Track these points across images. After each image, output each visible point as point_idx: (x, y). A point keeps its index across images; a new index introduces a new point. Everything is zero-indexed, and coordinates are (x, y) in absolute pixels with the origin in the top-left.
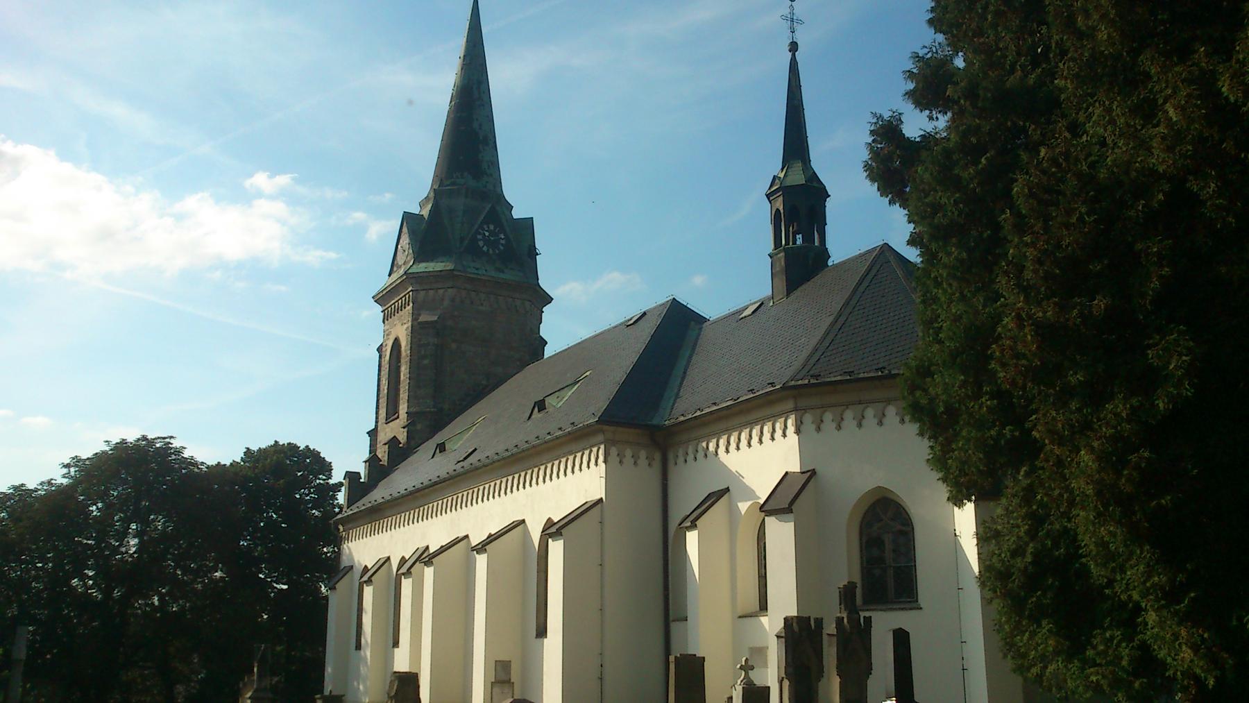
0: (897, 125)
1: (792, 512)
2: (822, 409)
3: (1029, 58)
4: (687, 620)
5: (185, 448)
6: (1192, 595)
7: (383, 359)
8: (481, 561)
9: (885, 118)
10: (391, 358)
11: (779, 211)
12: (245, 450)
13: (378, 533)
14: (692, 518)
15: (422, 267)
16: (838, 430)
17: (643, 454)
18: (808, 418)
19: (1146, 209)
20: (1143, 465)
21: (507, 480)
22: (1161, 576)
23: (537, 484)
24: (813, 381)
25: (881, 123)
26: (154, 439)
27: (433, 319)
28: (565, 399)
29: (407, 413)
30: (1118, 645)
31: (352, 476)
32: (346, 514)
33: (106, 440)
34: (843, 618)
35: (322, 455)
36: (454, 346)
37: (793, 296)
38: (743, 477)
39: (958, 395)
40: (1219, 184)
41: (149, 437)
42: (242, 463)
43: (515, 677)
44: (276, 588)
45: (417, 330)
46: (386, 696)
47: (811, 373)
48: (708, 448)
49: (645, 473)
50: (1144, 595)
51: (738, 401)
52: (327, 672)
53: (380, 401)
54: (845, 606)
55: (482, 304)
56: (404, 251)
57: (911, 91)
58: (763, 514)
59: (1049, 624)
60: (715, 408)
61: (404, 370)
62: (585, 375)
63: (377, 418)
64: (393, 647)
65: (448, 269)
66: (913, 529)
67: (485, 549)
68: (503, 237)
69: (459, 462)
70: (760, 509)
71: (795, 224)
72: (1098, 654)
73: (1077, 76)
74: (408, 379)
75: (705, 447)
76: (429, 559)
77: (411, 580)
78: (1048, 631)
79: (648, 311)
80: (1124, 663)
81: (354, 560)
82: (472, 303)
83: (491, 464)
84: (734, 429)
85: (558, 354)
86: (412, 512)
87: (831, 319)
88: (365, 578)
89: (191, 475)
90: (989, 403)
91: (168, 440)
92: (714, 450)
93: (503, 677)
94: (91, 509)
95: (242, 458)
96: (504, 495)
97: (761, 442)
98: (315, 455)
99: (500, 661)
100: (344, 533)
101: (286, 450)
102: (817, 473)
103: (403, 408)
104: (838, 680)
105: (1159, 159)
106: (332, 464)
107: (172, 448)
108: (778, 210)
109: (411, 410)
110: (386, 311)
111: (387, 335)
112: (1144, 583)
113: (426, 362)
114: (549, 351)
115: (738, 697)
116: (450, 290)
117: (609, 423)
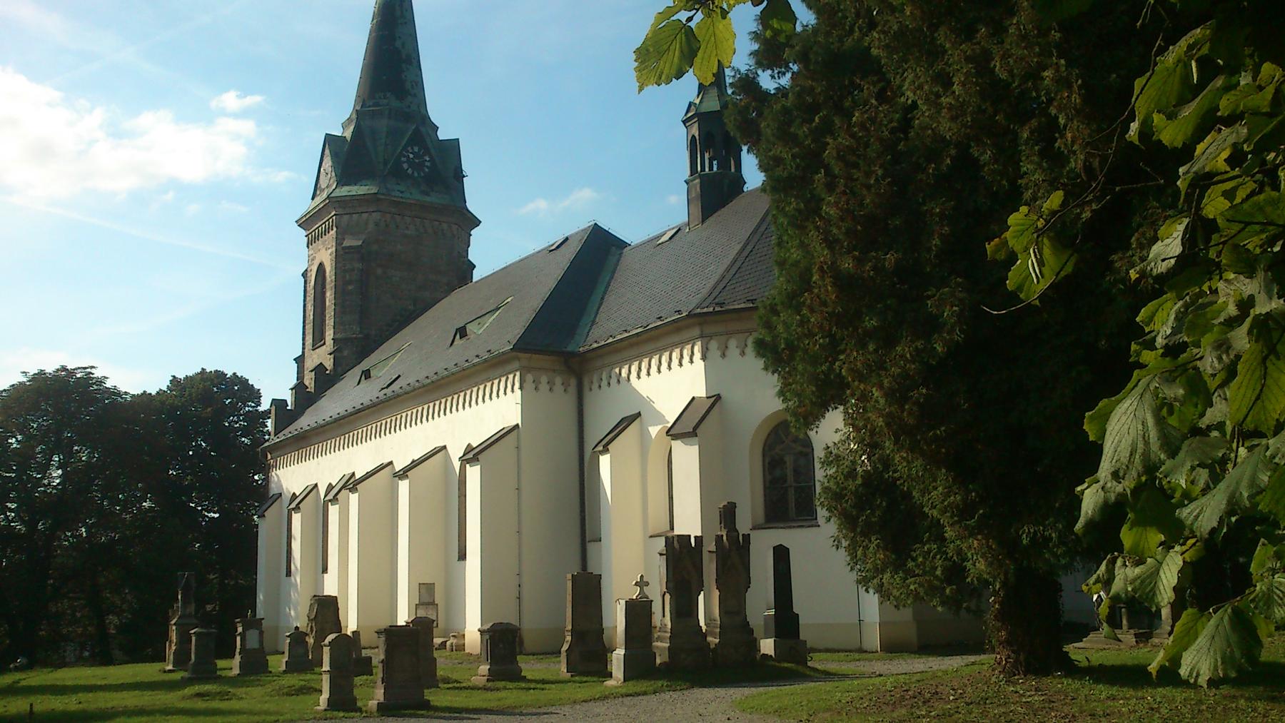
0: (754, 78)
1: (697, 436)
2: (727, 336)
3: (866, 20)
4: (600, 541)
5: (107, 378)
6: (981, 511)
7: (308, 285)
8: (404, 486)
9: (742, 72)
10: (316, 284)
11: (695, 137)
12: (171, 378)
13: (305, 461)
14: (604, 442)
15: (344, 191)
16: (723, 358)
17: (558, 380)
18: (713, 345)
19: (936, 172)
20: (922, 400)
21: (429, 407)
22: (957, 496)
23: (457, 410)
24: (718, 309)
25: (739, 76)
26: (74, 369)
27: (355, 244)
28: (485, 326)
29: (333, 339)
30: (934, 558)
31: (279, 404)
32: (273, 442)
33: (23, 371)
34: (722, 536)
35: (250, 382)
36: (379, 271)
37: (708, 222)
38: (654, 403)
39: (797, 333)
40: (994, 151)
41: (69, 368)
42: (169, 392)
43: (439, 599)
44: (207, 516)
45: (341, 255)
46: (307, 618)
47: (717, 300)
48: (620, 374)
49: (562, 400)
50: (944, 511)
51: (648, 328)
52: (260, 599)
53: (306, 327)
54: (724, 525)
55: (407, 228)
56: (327, 174)
57: (756, 51)
58: (669, 437)
59: (876, 540)
60: (627, 335)
61: (329, 295)
62: (506, 302)
63: (304, 344)
64: (323, 573)
65: (372, 192)
66: (813, 449)
67: (407, 475)
68: (428, 159)
69: (383, 389)
70: (667, 433)
71: (711, 150)
72: (918, 566)
73: (887, 46)
74: (333, 305)
75: (618, 372)
76: (354, 485)
77: (337, 506)
78: (876, 545)
79: (571, 236)
80: (938, 572)
81: (283, 489)
82: (397, 226)
83: (412, 391)
84: (665, 349)
85: (483, 278)
86: (338, 439)
87: (738, 247)
88: (293, 505)
89: (114, 403)
90: (821, 341)
91: (89, 370)
92: (626, 376)
93: (427, 600)
94: (10, 441)
95: (168, 386)
96: (456, 412)
97: (670, 367)
98: (244, 383)
99: (424, 584)
100: (272, 461)
101: (213, 377)
102: (722, 397)
103: (329, 334)
104: (717, 593)
105: (946, 127)
106: (261, 391)
107: (93, 378)
108: (693, 136)
109: (338, 336)
110: (310, 236)
111: (313, 260)
112: (944, 501)
113: (350, 287)
114: (477, 275)
115: (621, 610)
116: (374, 214)
117: (525, 351)
